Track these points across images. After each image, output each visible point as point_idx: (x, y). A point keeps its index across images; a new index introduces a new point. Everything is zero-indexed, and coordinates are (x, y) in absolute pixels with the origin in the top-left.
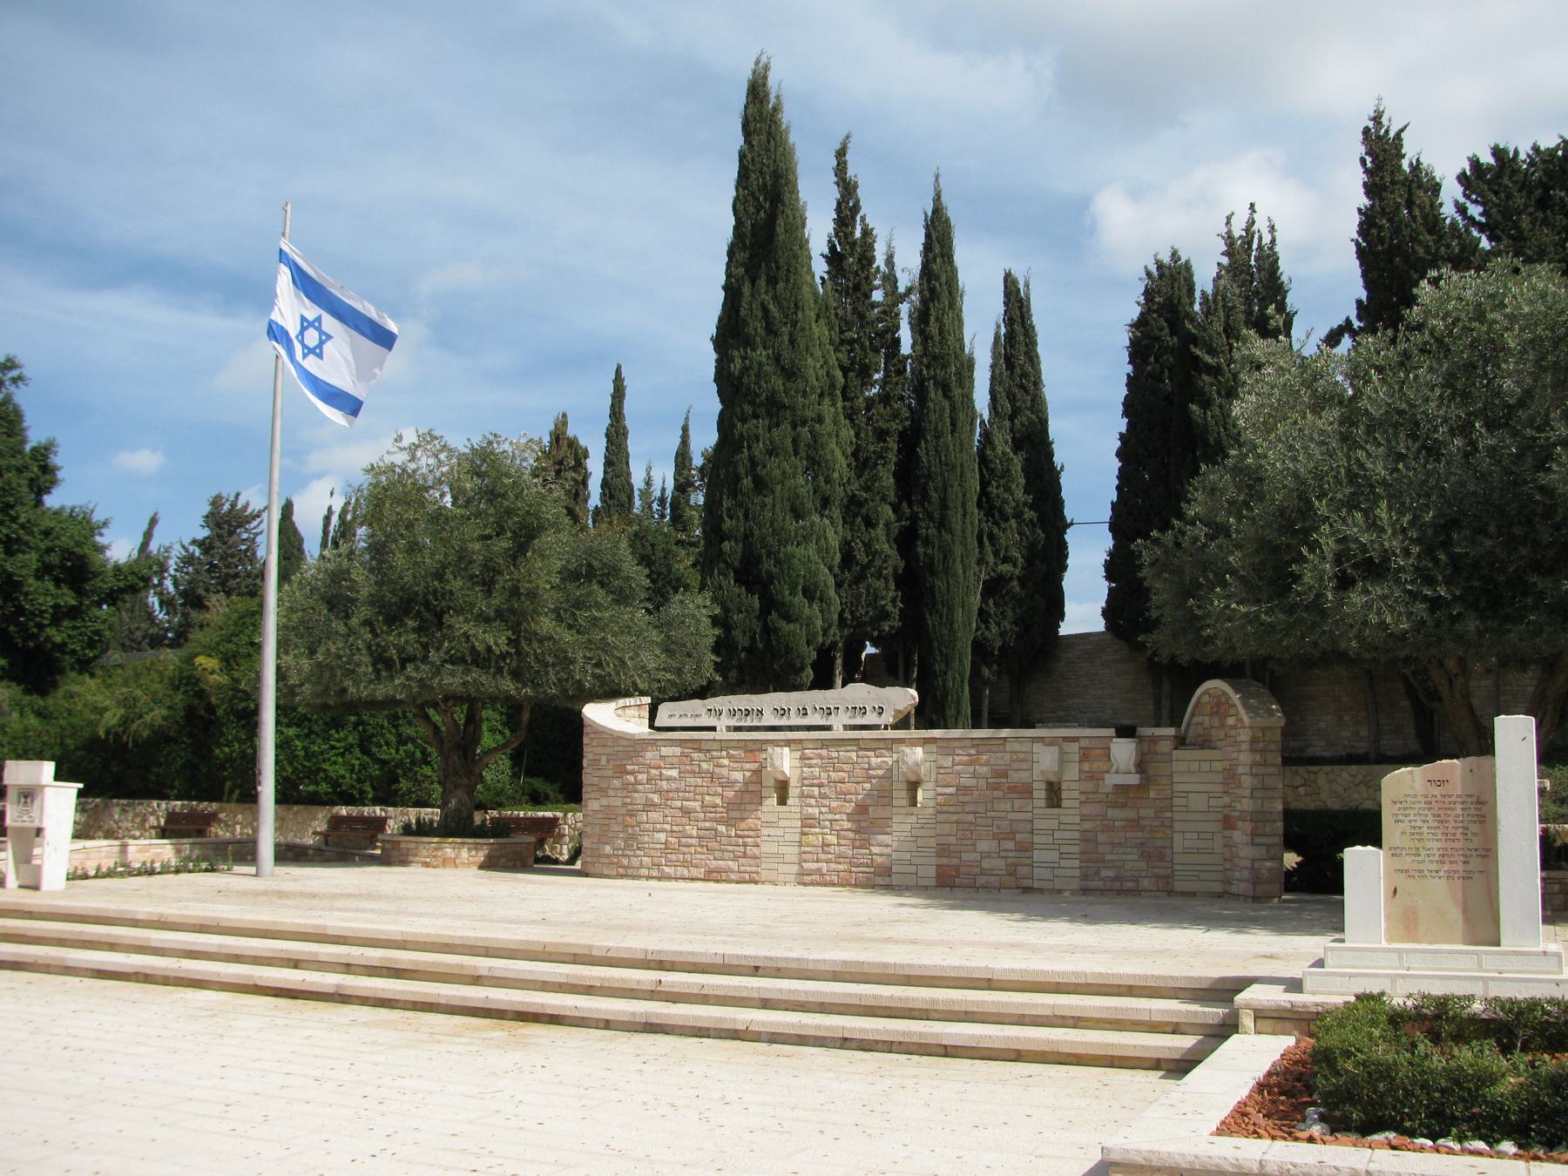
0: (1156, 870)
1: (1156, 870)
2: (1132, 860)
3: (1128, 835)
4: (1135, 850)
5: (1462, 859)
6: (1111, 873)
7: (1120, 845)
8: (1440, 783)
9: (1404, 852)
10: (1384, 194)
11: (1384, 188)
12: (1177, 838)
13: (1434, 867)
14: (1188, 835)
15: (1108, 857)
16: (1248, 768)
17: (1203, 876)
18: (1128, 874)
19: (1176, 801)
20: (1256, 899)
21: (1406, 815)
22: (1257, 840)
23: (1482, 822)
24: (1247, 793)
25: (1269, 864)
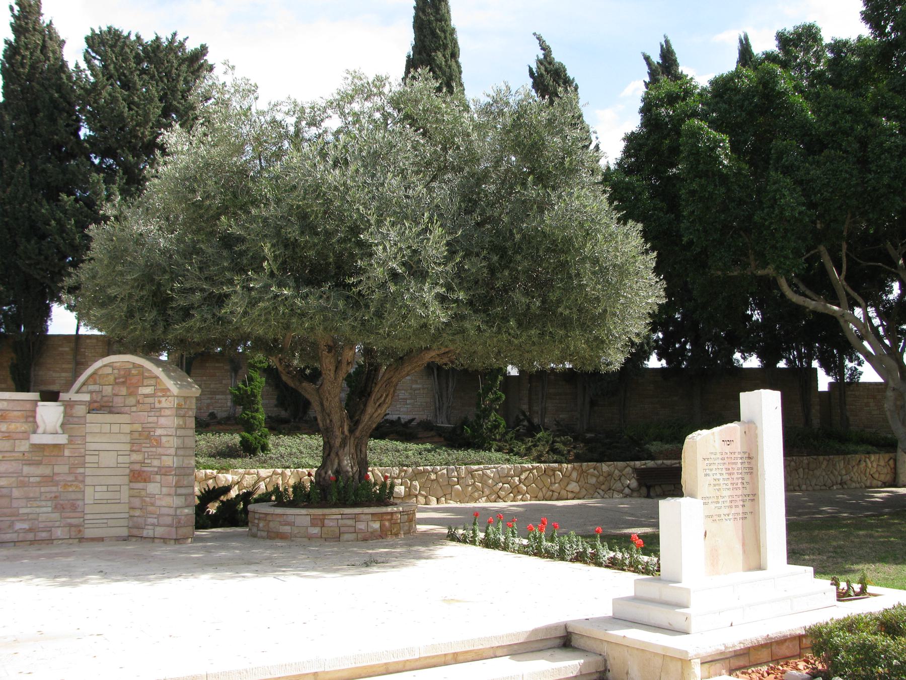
0: (69, 521)
1: (69, 521)
2: (45, 512)
3: (43, 489)
4: (49, 503)
5: (741, 503)
6: (26, 526)
7: (35, 499)
8: (729, 442)
9: (710, 501)
10: (27, 34)
11: (27, 30)
12: (89, 491)
13: (726, 511)
14: (98, 488)
15: (22, 511)
16: (174, 430)
17: (111, 523)
18: (41, 525)
19: (88, 459)
20: (177, 541)
21: (711, 470)
22: (180, 491)
23: (751, 473)
24: (172, 451)
25: (186, 511)
